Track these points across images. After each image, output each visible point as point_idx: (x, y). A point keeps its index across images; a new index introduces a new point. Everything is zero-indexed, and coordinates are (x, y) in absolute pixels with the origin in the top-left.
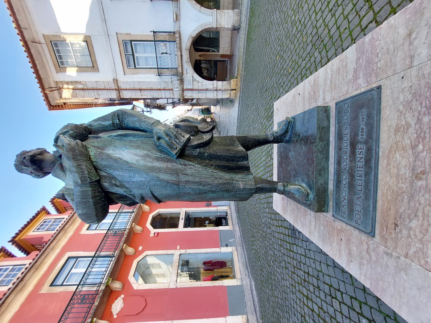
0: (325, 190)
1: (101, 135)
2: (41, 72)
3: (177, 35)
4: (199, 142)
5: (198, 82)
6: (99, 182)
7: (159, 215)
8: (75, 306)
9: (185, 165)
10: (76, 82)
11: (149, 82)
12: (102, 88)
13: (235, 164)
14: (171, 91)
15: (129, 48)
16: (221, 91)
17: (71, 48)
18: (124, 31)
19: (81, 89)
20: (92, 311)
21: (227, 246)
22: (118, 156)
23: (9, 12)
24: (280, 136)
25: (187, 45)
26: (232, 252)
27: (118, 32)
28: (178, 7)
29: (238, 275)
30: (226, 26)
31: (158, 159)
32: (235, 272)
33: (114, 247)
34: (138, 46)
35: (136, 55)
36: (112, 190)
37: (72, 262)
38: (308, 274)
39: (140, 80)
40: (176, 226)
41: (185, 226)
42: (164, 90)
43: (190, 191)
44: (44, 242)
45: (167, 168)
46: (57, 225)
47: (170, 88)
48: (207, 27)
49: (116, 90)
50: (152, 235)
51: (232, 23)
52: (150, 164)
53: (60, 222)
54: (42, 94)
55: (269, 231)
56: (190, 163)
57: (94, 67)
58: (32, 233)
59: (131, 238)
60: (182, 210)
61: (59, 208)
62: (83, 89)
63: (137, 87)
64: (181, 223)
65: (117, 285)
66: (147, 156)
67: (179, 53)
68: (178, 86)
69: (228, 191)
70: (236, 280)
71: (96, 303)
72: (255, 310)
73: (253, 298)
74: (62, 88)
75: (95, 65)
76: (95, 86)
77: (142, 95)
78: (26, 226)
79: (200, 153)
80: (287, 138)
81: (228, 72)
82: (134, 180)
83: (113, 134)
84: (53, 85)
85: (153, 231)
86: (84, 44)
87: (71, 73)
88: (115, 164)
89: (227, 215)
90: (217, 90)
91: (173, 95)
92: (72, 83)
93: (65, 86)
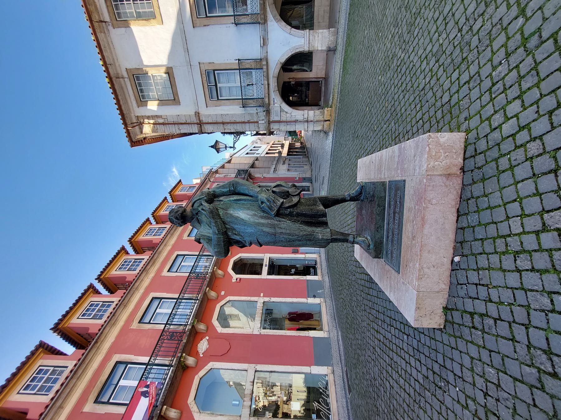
0: (382, 243)
1: (221, 198)
2: (123, 108)
3: (264, 63)
4: (290, 204)
5: (287, 113)
6: (226, 232)
7: (241, 260)
8: (165, 341)
9: (279, 221)
10: (157, 116)
11: (232, 115)
12: (183, 122)
13: (317, 220)
14: (256, 124)
15: (212, 78)
16: (312, 123)
17: (152, 81)
18: (207, 60)
19: (161, 124)
20: (181, 347)
21: (314, 297)
22: (237, 215)
23: (97, 50)
24: (356, 196)
25: (276, 71)
26: (321, 304)
27: (201, 62)
28: (266, 31)
29: (325, 327)
30: (320, 49)
31: (262, 217)
32: (322, 325)
33: (197, 290)
34: (221, 75)
35: (219, 85)
36: (232, 237)
37: (156, 303)
38: (378, 311)
39: (223, 113)
40: (260, 273)
41: (269, 273)
42: (249, 122)
43: (283, 239)
44: (128, 282)
45: (268, 223)
46: (138, 265)
47: (255, 120)
48: (297, 51)
49: (197, 124)
50: (234, 280)
51: (326, 44)
52: (257, 221)
53: (140, 262)
54: (125, 130)
55: (353, 278)
56: (283, 220)
57: (175, 101)
58: (115, 272)
59: (213, 281)
60: (266, 256)
61: (137, 248)
62: (163, 124)
63: (220, 120)
64: (265, 269)
65: (202, 327)
66: (255, 215)
67: (266, 82)
68: (264, 118)
69: (310, 240)
70: (322, 332)
71: (185, 341)
72: (341, 359)
73: (339, 348)
74: (143, 123)
75: (176, 98)
76: (176, 120)
77: (225, 129)
78: (109, 265)
79: (290, 212)
80: (362, 198)
81: (323, 94)
82: (247, 231)
83: (231, 199)
84: (135, 121)
85: (235, 277)
86: (165, 75)
87: (153, 106)
88: (235, 221)
89: (316, 264)
90: (307, 121)
91: (259, 128)
92: (152, 117)
93: (146, 121)
